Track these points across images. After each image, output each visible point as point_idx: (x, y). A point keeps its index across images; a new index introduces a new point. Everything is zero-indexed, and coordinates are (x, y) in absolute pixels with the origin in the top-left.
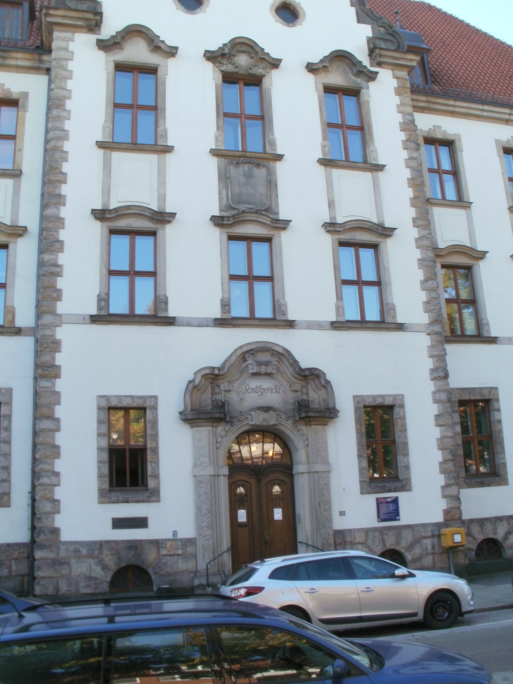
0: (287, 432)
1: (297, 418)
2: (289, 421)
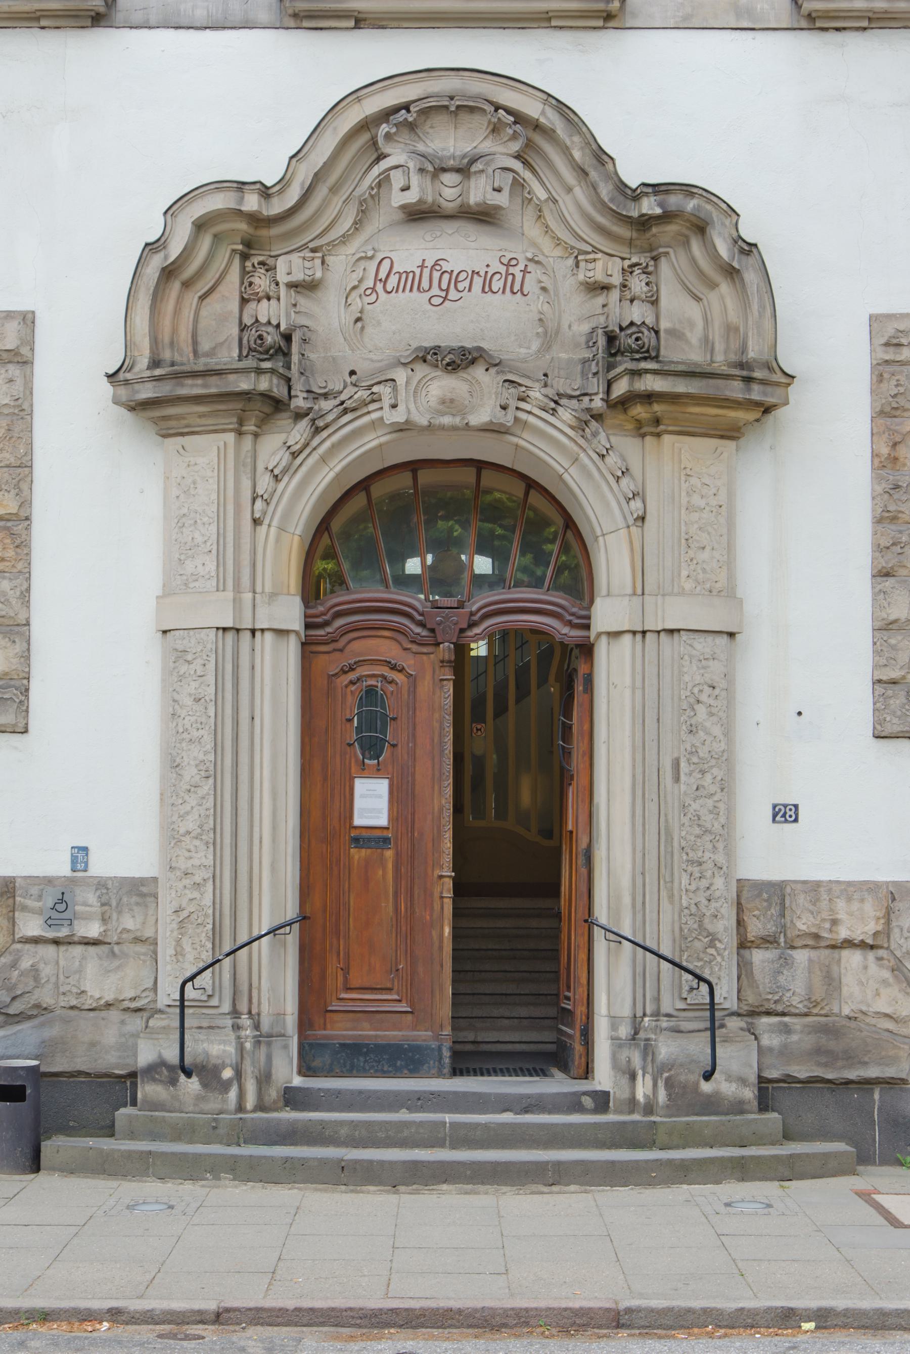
0: (556, 461)
1: (598, 403)
2: (560, 410)
